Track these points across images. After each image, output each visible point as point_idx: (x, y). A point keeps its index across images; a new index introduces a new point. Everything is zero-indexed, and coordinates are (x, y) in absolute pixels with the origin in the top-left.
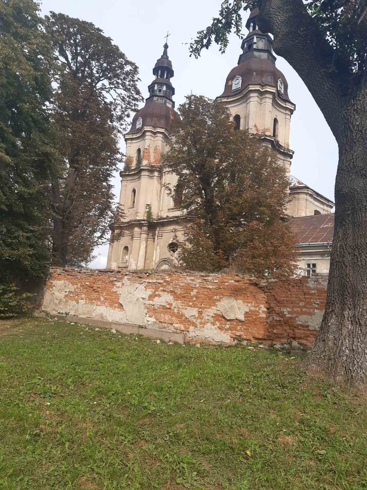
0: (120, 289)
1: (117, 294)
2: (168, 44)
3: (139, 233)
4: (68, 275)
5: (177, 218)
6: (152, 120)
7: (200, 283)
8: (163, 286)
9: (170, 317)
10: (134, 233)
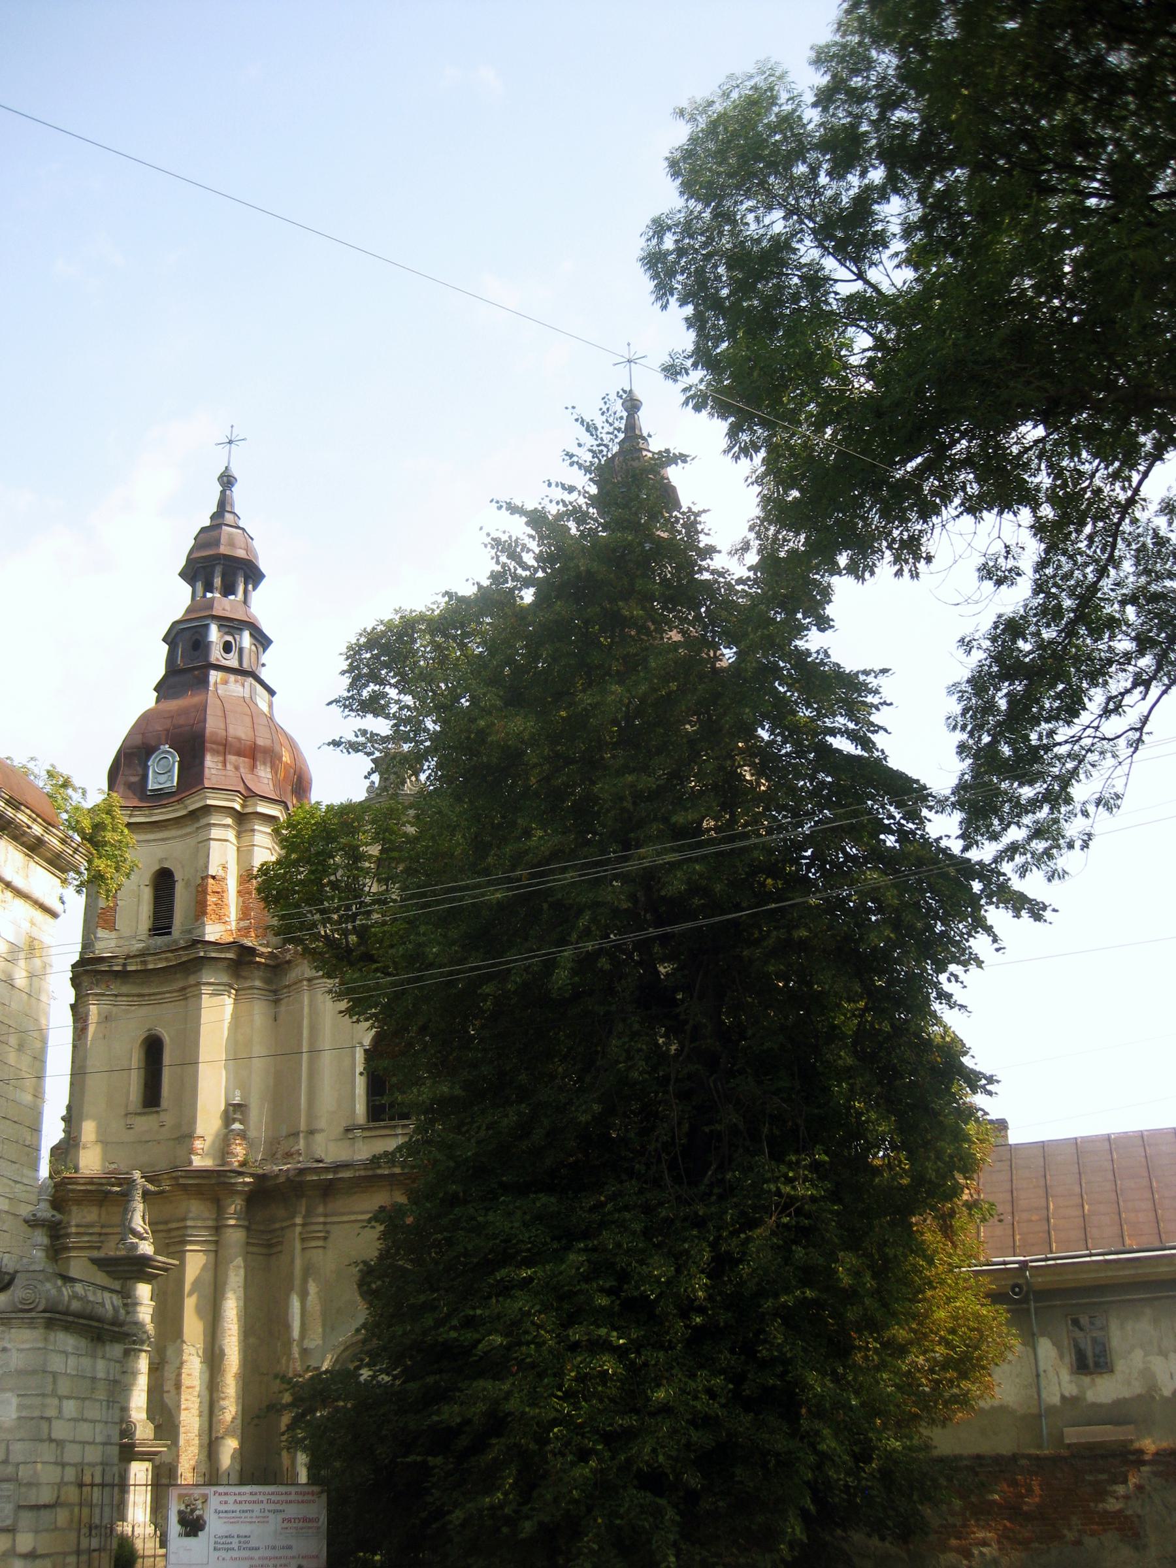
2: (235, 471)
5: (120, 1185)
6: (224, 763)
10: (189, 1223)
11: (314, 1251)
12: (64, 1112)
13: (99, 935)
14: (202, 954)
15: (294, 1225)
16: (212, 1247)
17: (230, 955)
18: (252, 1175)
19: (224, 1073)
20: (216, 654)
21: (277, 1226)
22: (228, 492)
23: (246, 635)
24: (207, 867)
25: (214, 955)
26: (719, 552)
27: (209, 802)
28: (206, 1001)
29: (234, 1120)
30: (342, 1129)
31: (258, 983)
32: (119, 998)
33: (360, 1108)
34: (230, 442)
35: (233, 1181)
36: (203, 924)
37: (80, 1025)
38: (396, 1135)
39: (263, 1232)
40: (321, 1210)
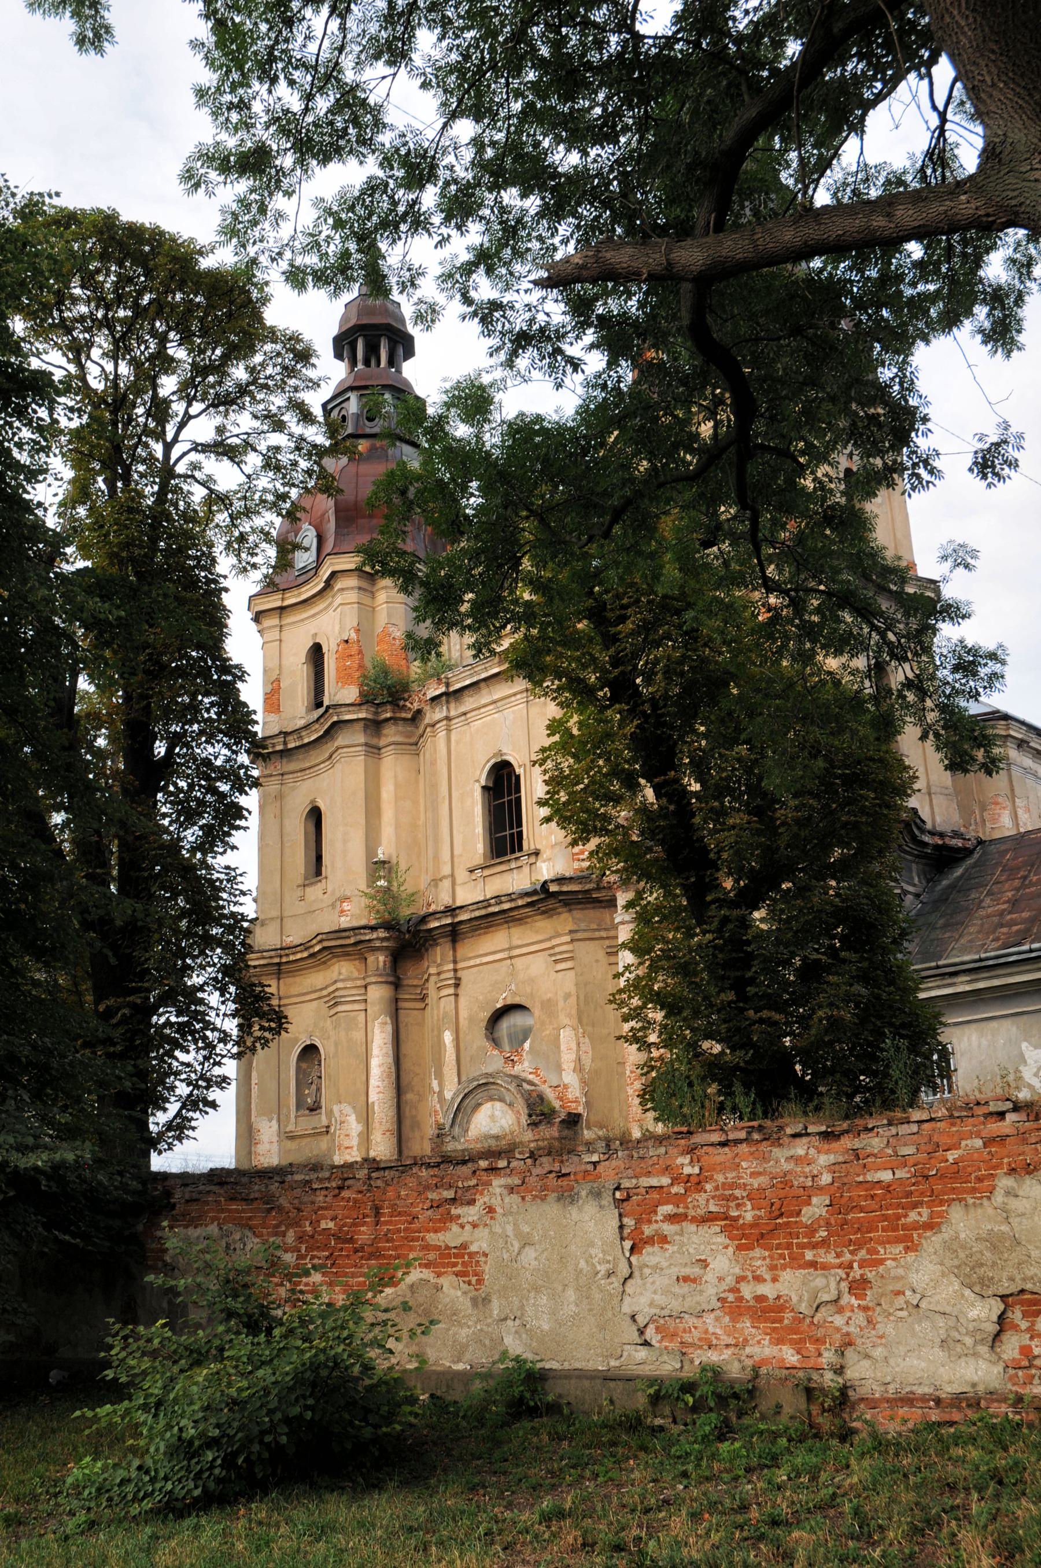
0: (482, 1233)
1: (471, 1255)
3: (359, 983)
4: (233, 1199)
7: (837, 1167)
8: (677, 1200)
9: (727, 1319)
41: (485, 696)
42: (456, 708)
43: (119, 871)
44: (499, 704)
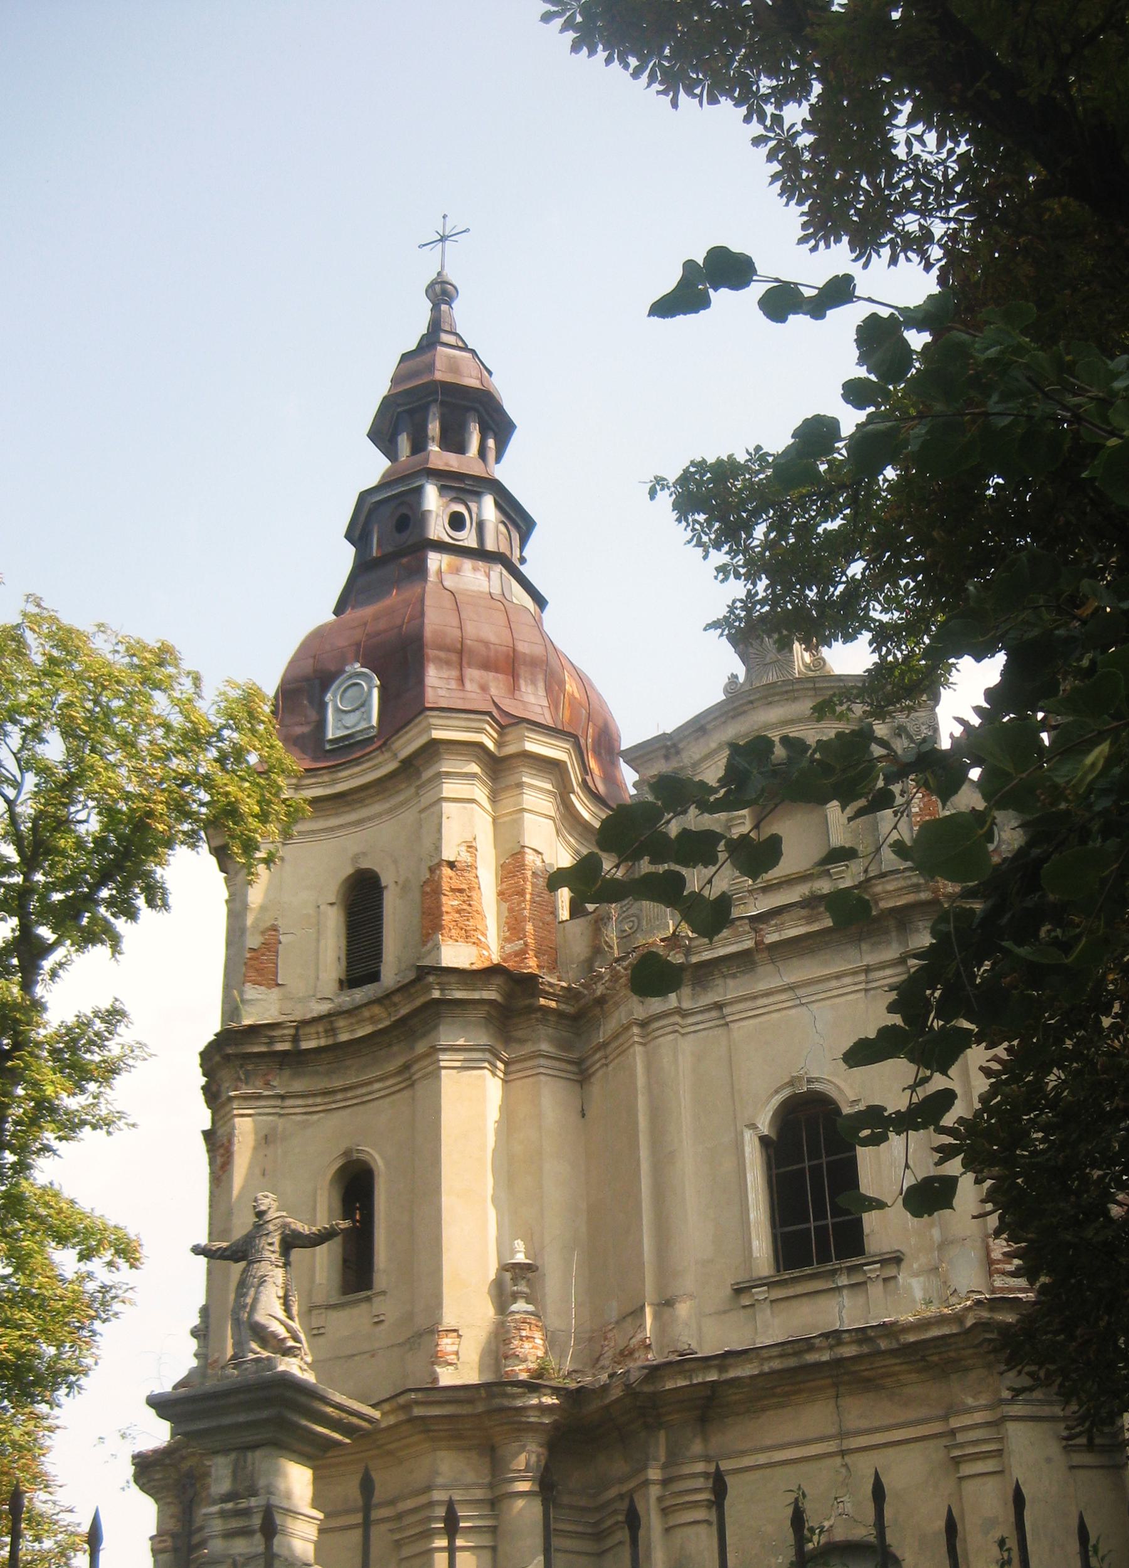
2: (451, 276)
6: (461, 680)
11: (690, 1531)
12: (196, 1321)
13: (247, 996)
14: (436, 994)
15: (646, 1483)
16: (486, 1540)
17: (490, 994)
18: (556, 1391)
19: (492, 1213)
20: (438, 529)
21: (612, 1493)
22: (444, 307)
23: (488, 502)
24: (438, 848)
25: (459, 995)
26: (880, 1205)
27: (437, 734)
28: (448, 1078)
29: (515, 1297)
30: (729, 1291)
31: (545, 1047)
32: (289, 1102)
33: (761, 1246)
34: (443, 239)
35: (519, 1403)
36: (437, 947)
37: (219, 1160)
38: (838, 1289)
39: (584, 1509)
40: (697, 1447)
41: (767, 979)
42: (694, 997)
43: (941, 995)
44: (800, 992)
